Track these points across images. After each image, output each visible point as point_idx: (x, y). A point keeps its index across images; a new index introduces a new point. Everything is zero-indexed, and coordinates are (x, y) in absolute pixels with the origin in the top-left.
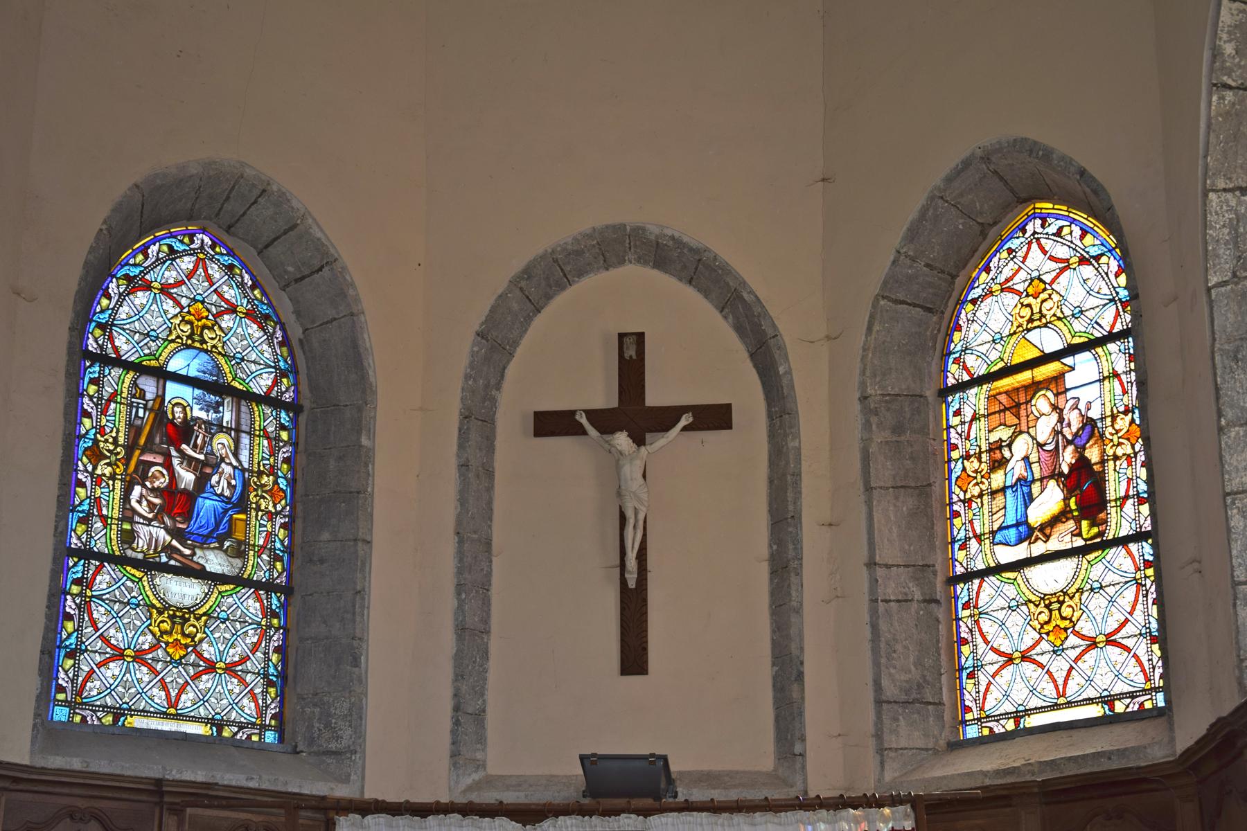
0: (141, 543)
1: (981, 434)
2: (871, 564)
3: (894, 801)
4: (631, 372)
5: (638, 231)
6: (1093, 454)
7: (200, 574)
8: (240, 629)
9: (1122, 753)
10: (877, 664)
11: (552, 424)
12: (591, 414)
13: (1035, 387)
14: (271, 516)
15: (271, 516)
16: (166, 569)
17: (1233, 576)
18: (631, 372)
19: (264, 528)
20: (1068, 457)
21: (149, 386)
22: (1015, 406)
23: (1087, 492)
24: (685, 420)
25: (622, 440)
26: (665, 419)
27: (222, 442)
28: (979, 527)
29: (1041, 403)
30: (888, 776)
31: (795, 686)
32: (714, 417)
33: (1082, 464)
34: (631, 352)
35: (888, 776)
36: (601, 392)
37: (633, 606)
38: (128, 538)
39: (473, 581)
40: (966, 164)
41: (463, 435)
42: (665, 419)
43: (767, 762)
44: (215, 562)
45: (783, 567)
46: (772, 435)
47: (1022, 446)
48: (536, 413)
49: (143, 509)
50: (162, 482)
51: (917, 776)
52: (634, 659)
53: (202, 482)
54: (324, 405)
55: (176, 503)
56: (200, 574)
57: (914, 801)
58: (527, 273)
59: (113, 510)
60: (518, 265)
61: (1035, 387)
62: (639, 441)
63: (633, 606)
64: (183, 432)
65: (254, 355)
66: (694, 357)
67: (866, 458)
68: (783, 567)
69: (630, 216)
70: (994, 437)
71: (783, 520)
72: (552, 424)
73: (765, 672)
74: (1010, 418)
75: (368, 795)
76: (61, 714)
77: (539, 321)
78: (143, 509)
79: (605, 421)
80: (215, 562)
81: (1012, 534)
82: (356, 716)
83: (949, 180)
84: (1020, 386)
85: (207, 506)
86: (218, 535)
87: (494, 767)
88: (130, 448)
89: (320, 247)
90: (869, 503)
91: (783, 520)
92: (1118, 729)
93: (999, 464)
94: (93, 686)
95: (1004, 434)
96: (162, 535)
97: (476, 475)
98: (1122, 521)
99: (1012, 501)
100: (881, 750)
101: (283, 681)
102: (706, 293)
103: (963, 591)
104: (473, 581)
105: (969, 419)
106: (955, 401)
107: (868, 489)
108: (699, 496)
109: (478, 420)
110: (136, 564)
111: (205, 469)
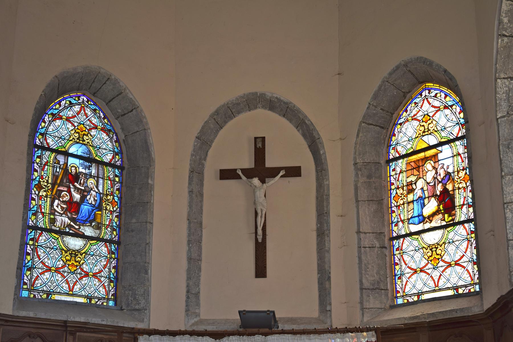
0: (58, 224)
1: (404, 179)
2: (358, 232)
3: (368, 330)
4: (260, 153)
5: (263, 95)
6: (450, 187)
7: (82, 236)
8: (99, 259)
9: (462, 310)
10: (361, 273)
11: (227, 174)
12: (243, 171)
13: (426, 159)
14: (112, 212)
15: (112, 212)
16: (68, 234)
17: (507, 237)
18: (260, 153)
19: (109, 217)
20: (439, 188)
21: (61, 159)
22: (418, 167)
23: (447, 203)
24: (282, 173)
25: (256, 181)
26: (273, 172)
27: (91, 182)
28: (403, 217)
29: (428, 166)
30: (365, 319)
31: (327, 283)
32: (294, 172)
33: (445, 191)
34: (260, 145)
35: (365, 319)
36: (247, 161)
37: (261, 249)
38: (53, 221)
39: (195, 239)
40: (398, 67)
41: (191, 179)
42: (273, 172)
43: (315, 314)
44: (88, 231)
45: (322, 233)
46: (318, 179)
47: (420, 183)
48: (221, 170)
49: (59, 210)
50: (67, 198)
51: (377, 319)
52: (261, 271)
53: (83, 198)
54: (133, 167)
55: (72, 207)
56: (82, 236)
57: (376, 330)
58: (217, 112)
59: (47, 210)
60: (213, 109)
61: (426, 159)
62: (263, 182)
63: (261, 249)
64: (75, 178)
65: (105, 146)
66: (286, 147)
67: (356, 189)
68: (322, 233)
69: (259, 89)
70: (409, 180)
71: (322, 214)
72: (227, 174)
73: (315, 276)
74: (416, 172)
75: (152, 327)
76: (25, 294)
77: (222, 132)
78: (59, 210)
79: (249, 173)
80: (88, 231)
81: (416, 220)
82: (147, 294)
83: (390, 74)
84: (420, 159)
85: (85, 208)
86: (90, 220)
87: (203, 316)
88: (53, 185)
89: (132, 102)
90: (357, 207)
91: (322, 214)
92: (460, 300)
93: (411, 191)
94: (38, 283)
95: (413, 178)
96: (67, 220)
97: (196, 196)
98: (461, 214)
99: (416, 206)
100: (362, 309)
101: (116, 280)
102: (290, 121)
103: (396, 243)
104: (195, 239)
105: (399, 173)
106: (393, 165)
107: (357, 201)
108: (288, 204)
109: (196, 173)
110: (56, 232)
111: (84, 193)
